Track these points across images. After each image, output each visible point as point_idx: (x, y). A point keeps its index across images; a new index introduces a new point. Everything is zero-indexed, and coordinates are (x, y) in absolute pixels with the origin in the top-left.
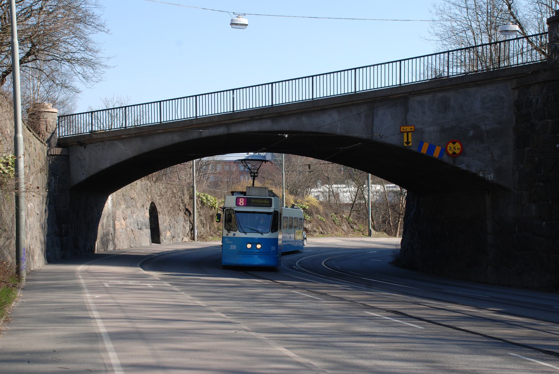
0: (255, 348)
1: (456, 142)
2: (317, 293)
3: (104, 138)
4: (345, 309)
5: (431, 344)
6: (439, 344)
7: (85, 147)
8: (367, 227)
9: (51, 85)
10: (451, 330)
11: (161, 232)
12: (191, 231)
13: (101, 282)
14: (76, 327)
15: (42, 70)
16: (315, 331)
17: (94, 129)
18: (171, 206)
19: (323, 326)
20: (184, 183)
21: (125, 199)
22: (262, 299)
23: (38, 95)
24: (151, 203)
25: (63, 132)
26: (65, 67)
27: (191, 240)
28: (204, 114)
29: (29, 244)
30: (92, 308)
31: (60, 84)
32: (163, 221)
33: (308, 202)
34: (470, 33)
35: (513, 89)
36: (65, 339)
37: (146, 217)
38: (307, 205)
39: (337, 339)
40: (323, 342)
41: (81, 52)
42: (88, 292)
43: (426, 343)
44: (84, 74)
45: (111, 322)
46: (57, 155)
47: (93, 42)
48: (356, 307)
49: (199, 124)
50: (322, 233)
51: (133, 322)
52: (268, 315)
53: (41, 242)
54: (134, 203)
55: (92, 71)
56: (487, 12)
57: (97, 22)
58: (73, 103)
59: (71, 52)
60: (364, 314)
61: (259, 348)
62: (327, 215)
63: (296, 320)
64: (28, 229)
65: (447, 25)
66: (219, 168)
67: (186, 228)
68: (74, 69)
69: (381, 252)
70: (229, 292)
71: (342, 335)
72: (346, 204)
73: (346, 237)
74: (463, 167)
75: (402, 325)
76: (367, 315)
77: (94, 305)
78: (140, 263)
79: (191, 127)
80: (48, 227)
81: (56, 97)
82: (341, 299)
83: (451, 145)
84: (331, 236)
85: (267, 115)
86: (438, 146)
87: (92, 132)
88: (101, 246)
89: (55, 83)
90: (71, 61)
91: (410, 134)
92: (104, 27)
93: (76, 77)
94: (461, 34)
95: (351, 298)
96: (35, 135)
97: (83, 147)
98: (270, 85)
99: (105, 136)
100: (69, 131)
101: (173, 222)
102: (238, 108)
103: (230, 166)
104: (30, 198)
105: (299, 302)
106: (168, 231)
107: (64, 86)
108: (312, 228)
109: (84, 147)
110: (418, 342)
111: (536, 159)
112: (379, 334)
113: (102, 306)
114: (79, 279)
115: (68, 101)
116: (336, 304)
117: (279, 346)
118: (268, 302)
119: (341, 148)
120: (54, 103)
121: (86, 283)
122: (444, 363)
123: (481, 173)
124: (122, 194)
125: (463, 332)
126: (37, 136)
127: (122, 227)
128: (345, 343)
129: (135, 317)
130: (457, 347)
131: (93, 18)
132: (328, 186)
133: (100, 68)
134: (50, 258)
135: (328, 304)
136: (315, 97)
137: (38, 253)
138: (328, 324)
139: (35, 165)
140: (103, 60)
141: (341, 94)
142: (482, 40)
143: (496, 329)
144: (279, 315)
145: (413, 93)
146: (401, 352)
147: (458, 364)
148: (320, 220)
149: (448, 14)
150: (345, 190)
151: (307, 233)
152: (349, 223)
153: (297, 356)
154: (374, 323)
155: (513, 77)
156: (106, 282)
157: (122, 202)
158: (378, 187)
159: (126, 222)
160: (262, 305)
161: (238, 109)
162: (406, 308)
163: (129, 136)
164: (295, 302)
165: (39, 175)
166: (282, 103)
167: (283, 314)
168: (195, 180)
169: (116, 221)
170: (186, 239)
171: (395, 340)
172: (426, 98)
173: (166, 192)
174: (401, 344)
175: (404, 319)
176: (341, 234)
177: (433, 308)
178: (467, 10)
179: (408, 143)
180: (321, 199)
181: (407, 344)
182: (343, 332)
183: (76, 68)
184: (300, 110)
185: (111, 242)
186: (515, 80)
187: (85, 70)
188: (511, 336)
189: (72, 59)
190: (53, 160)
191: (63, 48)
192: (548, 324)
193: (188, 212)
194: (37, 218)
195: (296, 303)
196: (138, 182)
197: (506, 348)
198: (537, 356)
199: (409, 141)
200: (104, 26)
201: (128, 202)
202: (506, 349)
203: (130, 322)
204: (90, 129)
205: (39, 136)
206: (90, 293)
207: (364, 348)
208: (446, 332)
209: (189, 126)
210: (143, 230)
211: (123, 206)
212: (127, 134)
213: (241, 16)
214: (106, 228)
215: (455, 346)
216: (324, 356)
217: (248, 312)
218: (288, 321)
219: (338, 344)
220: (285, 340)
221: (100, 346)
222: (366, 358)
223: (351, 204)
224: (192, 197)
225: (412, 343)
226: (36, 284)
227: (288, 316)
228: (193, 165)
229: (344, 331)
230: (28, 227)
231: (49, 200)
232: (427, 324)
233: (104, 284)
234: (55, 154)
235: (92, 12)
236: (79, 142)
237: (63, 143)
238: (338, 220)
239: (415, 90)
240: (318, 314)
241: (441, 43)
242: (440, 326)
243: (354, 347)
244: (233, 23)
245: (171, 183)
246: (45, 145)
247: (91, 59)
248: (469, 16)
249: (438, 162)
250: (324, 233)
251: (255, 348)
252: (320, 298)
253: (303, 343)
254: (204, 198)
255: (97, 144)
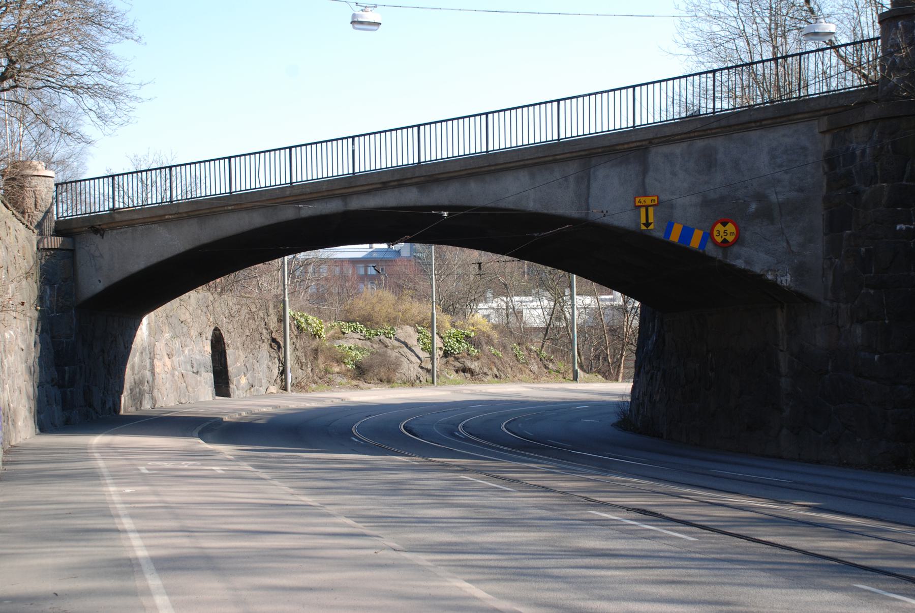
0: (414, 583)
1: (727, 223)
2: (504, 479)
3: (134, 220)
4: (555, 507)
5: (717, 569)
6: (731, 569)
7: (102, 236)
8: (570, 365)
9: (42, 131)
10: (744, 543)
11: (232, 378)
12: (282, 376)
13: (134, 465)
14: (93, 549)
15: (26, 105)
16: (512, 547)
17: (117, 206)
18: (248, 334)
19: (524, 538)
20: (269, 296)
21: (170, 324)
22: (412, 492)
23: (20, 149)
24: (214, 330)
25: (63, 211)
26: (68, 100)
27: (281, 391)
28: (310, 178)
29: (8, 401)
30: (121, 513)
31: (58, 129)
32: (235, 359)
33: (473, 325)
34: (741, 43)
35: (821, 132)
36: (74, 571)
37: (206, 353)
38: (473, 331)
39: (552, 562)
40: (529, 568)
41: (93, 74)
42: (111, 483)
43: (707, 569)
44: (99, 111)
45: (155, 537)
46: (55, 249)
47: (114, 58)
48: (573, 503)
49: (296, 196)
50: (497, 377)
51: (195, 536)
52: (425, 520)
53: (28, 397)
54: (185, 330)
55: (112, 106)
56: (769, 8)
57: (121, 24)
58: (80, 163)
59: (77, 75)
60: (589, 515)
61: (423, 583)
62: (505, 347)
63: (476, 529)
64: (6, 375)
65: (705, 30)
66: (324, 269)
67: (273, 371)
68: (82, 103)
69: (596, 408)
70: (354, 479)
71: (559, 555)
72: (535, 328)
73: (537, 383)
74: (740, 264)
75: (659, 535)
76: (595, 518)
77: (123, 506)
78: (198, 431)
79: (282, 200)
80: (41, 371)
81: (52, 151)
82: (547, 489)
83: (719, 227)
84: (512, 381)
85: (411, 178)
86: (698, 229)
87: (113, 210)
88: (130, 401)
89: (49, 127)
90: (76, 89)
91: (651, 210)
92: (131, 31)
93: (86, 118)
94: (726, 45)
95: (561, 487)
96: (15, 216)
97: (99, 235)
98: (416, 129)
99: (136, 216)
100: (75, 210)
101: (251, 360)
102: (360, 168)
103: (342, 267)
104: (9, 322)
105: (476, 496)
106: (243, 377)
107: (66, 132)
108: (481, 368)
109: (101, 235)
110: (693, 566)
111: (863, 249)
112: (622, 552)
113: (138, 507)
114: (95, 459)
115: (71, 160)
116: (538, 499)
117: (455, 578)
118: (422, 497)
119: (536, 235)
120: (48, 162)
121: (107, 468)
122: (748, 606)
123: (770, 273)
124: (164, 315)
125: (766, 546)
126: (20, 216)
127: (166, 370)
128: (568, 570)
129: (200, 528)
130: (763, 574)
131: (113, 16)
132: (505, 299)
133: (126, 101)
134: (45, 425)
135: (525, 499)
136: (490, 148)
137: (23, 416)
138: (532, 534)
139: (17, 266)
140: (132, 87)
141: (511, 147)
142: (761, 55)
143: (820, 541)
144: (445, 520)
145: (656, 141)
146: (668, 586)
147: (773, 608)
148: (494, 355)
149: (706, 11)
150: (534, 304)
151: (472, 376)
152: (541, 360)
153: (490, 596)
154: (610, 532)
155: (822, 112)
156: (142, 465)
157: (166, 328)
158: (588, 300)
159: (172, 362)
160: (413, 501)
161: (363, 170)
162: (659, 503)
163: (176, 216)
164: (468, 496)
165: (24, 282)
166: (437, 160)
167: (451, 518)
168: (287, 290)
169: (155, 361)
170: (273, 389)
171: (653, 562)
172: (677, 149)
173: (239, 311)
174: (665, 570)
175: (660, 523)
176: (528, 377)
177: (705, 504)
178: (738, 4)
179: (647, 224)
180: (494, 320)
181: (676, 570)
182: (559, 549)
183: (85, 102)
184: (466, 170)
185: (147, 396)
186: (827, 117)
187: (101, 104)
188: (850, 552)
189: (79, 85)
190: (47, 257)
191: (62, 67)
192: (904, 530)
193: (276, 344)
194: (20, 356)
195: (470, 498)
196: (192, 293)
197: (848, 575)
198: (904, 589)
199: (650, 221)
200: (132, 29)
201: (175, 328)
202: (847, 577)
203: (188, 536)
204: (111, 206)
205: (24, 217)
206: (116, 484)
207: (602, 579)
208: (737, 547)
209: (278, 198)
210: (201, 375)
211: (167, 335)
212: (174, 212)
213: (370, 9)
214: (140, 371)
215: (758, 573)
216: (534, 595)
217: (390, 515)
218: (461, 530)
219: (556, 572)
220: (462, 566)
221: (138, 583)
222: (609, 599)
223: (544, 328)
224: (282, 320)
225: (683, 568)
226: (21, 470)
227: (461, 521)
228: (284, 266)
229: (561, 547)
230: (6, 372)
231: (42, 326)
232: (700, 533)
233: (140, 468)
234: (50, 247)
235: (112, 6)
236: (93, 227)
237: (64, 229)
238: (523, 354)
239: (659, 136)
240: (511, 517)
241: (695, 58)
242: (723, 536)
243: (585, 577)
244: (356, 20)
245: (247, 295)
246: (34, 232)
247: (111, 87)
248: (741, 15)
249: (699, 257)
250: (501, 376)
251: (414, 583)
252: (509, 487)
253: (494, 571)
254: (303, 320)
255: (122, 230)
